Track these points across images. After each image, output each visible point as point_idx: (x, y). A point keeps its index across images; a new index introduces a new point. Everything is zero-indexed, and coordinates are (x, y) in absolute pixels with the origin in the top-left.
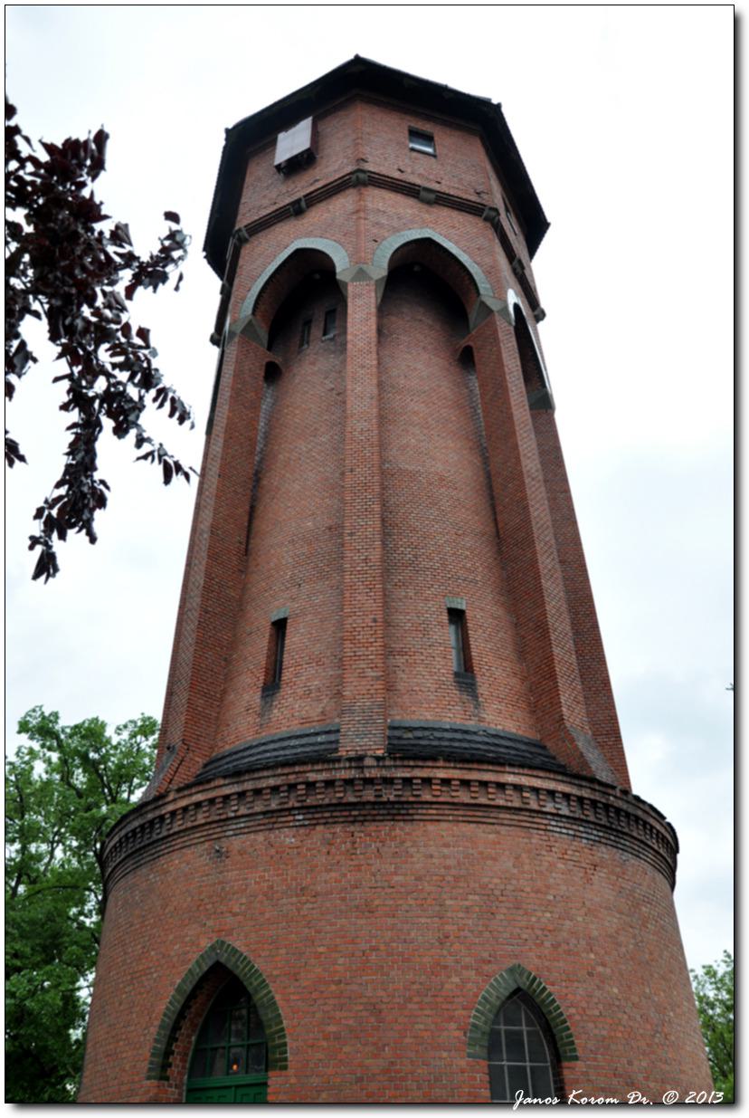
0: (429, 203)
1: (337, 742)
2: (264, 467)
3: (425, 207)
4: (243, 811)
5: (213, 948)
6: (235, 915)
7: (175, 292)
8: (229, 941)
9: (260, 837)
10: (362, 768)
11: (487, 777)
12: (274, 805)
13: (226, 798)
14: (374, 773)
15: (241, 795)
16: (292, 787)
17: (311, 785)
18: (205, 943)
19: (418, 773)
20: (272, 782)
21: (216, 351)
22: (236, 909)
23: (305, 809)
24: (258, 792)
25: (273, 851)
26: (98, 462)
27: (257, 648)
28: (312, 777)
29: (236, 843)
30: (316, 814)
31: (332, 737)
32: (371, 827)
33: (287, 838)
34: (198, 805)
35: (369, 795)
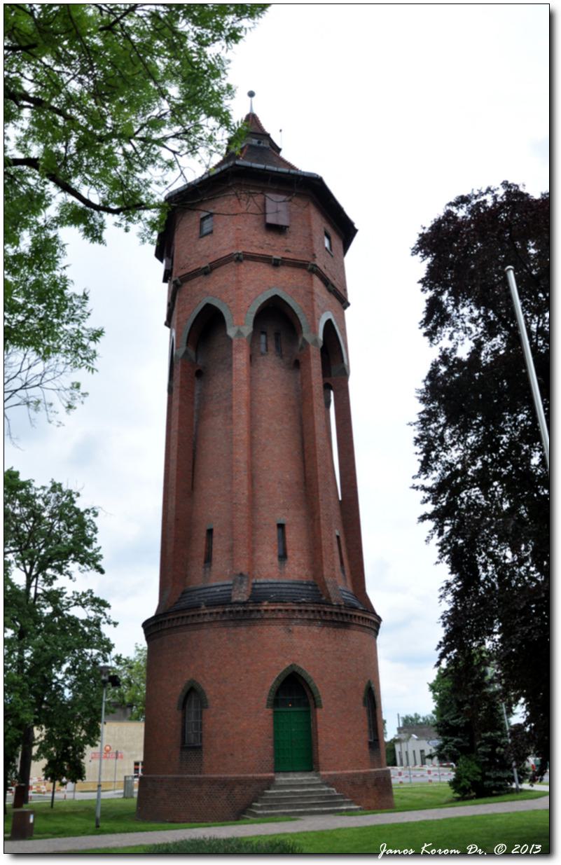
0: (330, 291)
1: (230, 594)
2: (256, 436)
3: (327, 292)
4: (299, 617)
5: (291, 666)
6: (299, 655)
7: (127, 233)
8: (297, 664)
9: (306, 628)
10: (340, 609)
11: (187, 614)
12: (312, 617)
13: (294, 611)
14: (343, 611)
15: (300, 611)
16: (319, 612)
17: (325, 612)
18: (288, 664)
19: (215, 610)
20: (312, 608)
21: (168, 330)
22: (299, 653)
23: (322, 620)
24: (306, 611)
25: (310, 634)
26: (425, 305)
27: (199, 547)
28: (326, 609)
29: (296, 628)
30: (326, 623)
31: (229, 592)
32: (340, 630)
33: (315, 630)
34: (280, 610)
35: (341, 619)
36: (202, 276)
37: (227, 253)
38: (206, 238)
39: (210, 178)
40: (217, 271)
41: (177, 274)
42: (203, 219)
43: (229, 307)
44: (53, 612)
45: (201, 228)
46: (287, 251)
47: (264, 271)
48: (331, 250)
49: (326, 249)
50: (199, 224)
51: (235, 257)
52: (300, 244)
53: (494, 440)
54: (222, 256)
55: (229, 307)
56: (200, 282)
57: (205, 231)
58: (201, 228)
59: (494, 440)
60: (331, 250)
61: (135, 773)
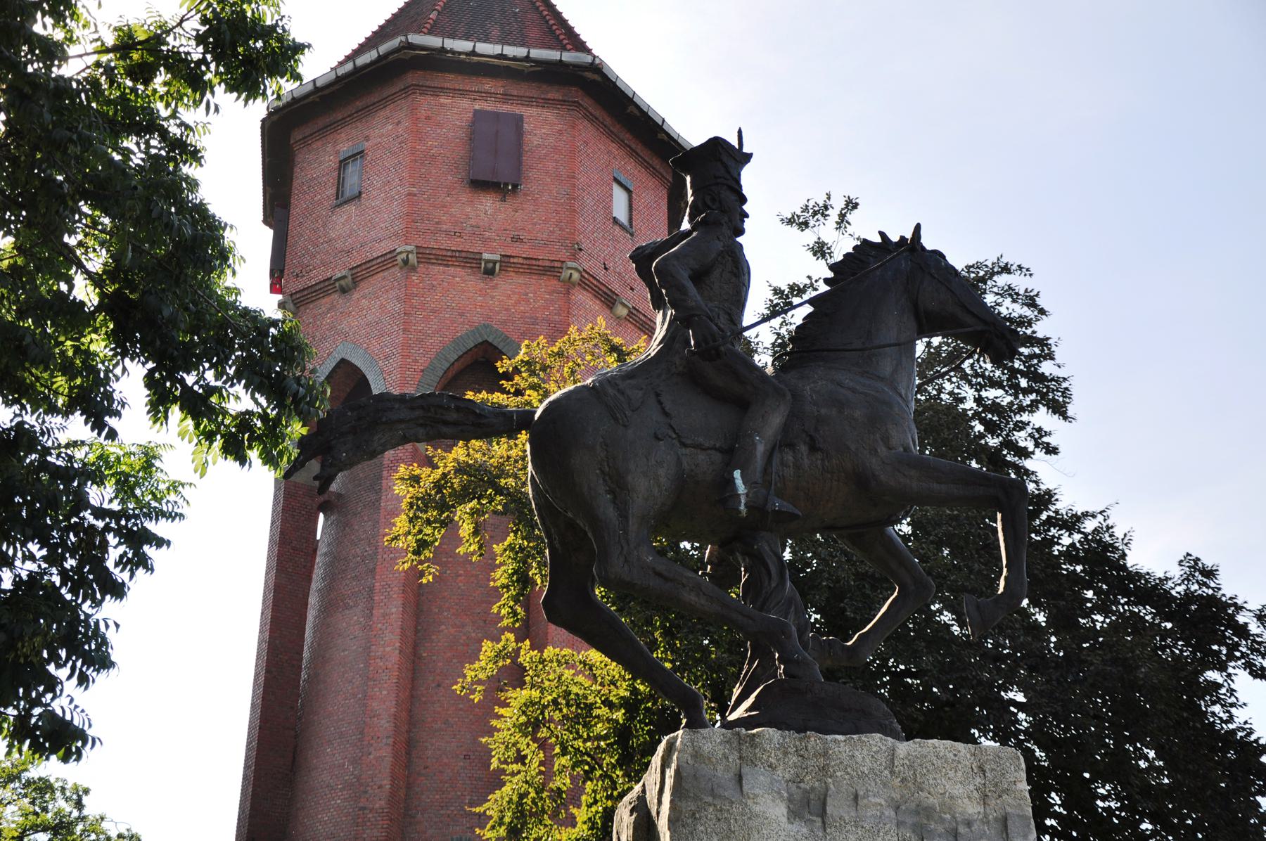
36: (336, 296)
37: (385, 247)
38: (346, 207)
39: (339, 79)
40: (366, 288)
41: (294, 285)
42: (343, 163)
43: (382, 372)
44: (923, 248)
45: (340, 182)
46: (516, 239)
47: (465, 283)
48: (631, 226)
49: (615, 221)
50: (335, 174)
51: (399, 258)
52: (546, 221)
53: (992, 727)
54: (375, 255)
55: (382, 372)
56: (332, 308)
57: (348, 194)
58: (340, 182)
59: (992, 727)
60: (631, 226)
61: (1082, 513)
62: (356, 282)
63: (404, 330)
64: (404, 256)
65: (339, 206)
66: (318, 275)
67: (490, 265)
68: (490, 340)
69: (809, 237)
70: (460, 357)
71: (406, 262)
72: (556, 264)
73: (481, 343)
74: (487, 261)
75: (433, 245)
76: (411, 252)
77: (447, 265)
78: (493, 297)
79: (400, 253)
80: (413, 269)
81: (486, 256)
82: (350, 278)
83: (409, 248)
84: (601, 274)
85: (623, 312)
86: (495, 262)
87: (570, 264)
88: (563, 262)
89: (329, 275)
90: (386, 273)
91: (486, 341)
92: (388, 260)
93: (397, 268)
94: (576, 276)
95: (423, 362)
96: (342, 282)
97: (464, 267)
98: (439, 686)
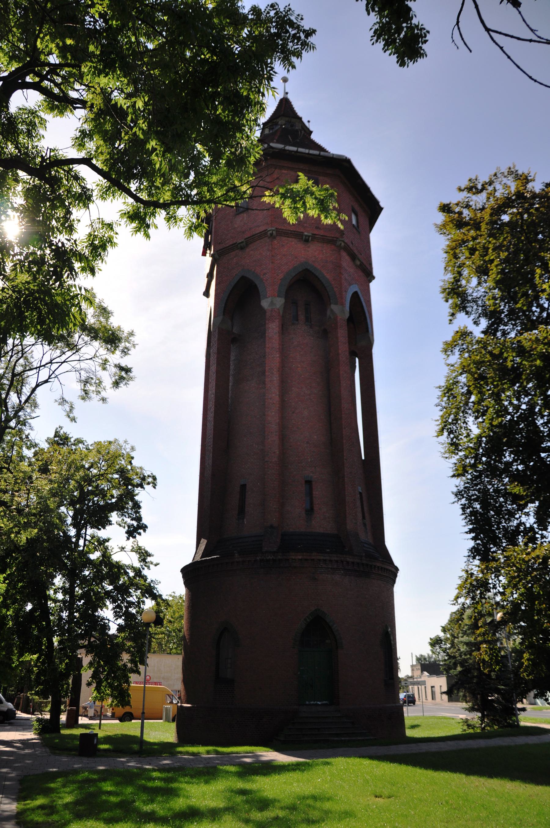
36: (238, 251)
37: (262, 229)
54: (257, 232)
62: (247, 245)
63: (272, 262)
64: (271, 232)
65: (238, 214)
66: (230, 242)
67: (307, 238)
68: (309, 268)
69: (79, 404)
70: (296, 275)
71: (272, 234)
72: (335, 239)
73: (304, 270)
74: (306, 236)
75: (283, 228)
76: (274, 230)
77: (288, 237)
78: (308, 251)
79: (270, 231)
80: (275, 238)
81: (306, 234)
82: (245, 243)
83: (273, 229)
84: (351, 246)
85: (358, 263)
86: (309, 236)
87: (341, 239)
88: (337, 238)
89: (235, 242)
90: (262, 240)
91: (307, 269)
92: (264, 234)
93: (267, 238)
94: (343, 244)
95: (281, 276)
96: (242, 245)
97: (295, 238)
98: (293, 413)
